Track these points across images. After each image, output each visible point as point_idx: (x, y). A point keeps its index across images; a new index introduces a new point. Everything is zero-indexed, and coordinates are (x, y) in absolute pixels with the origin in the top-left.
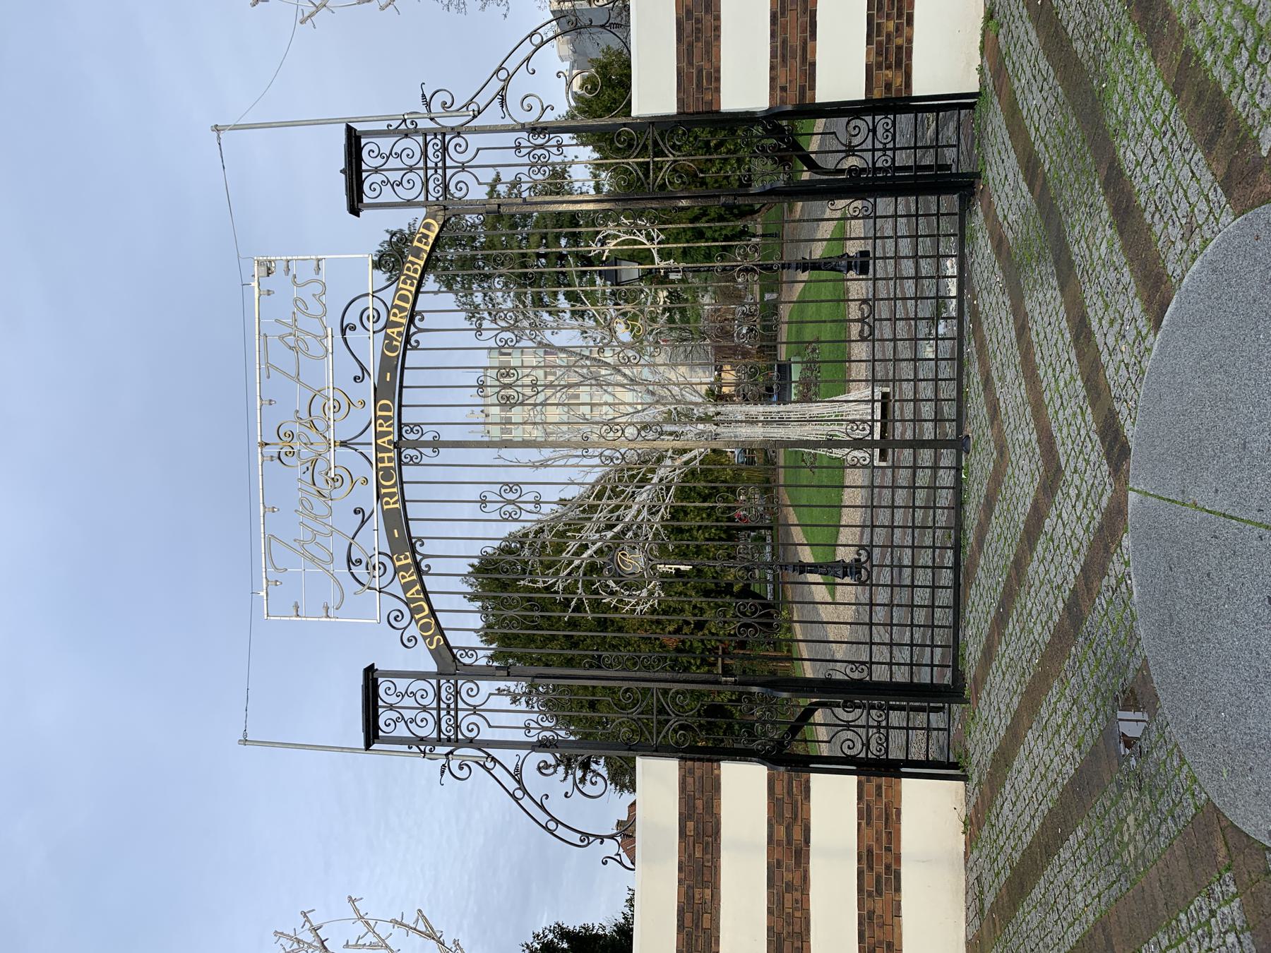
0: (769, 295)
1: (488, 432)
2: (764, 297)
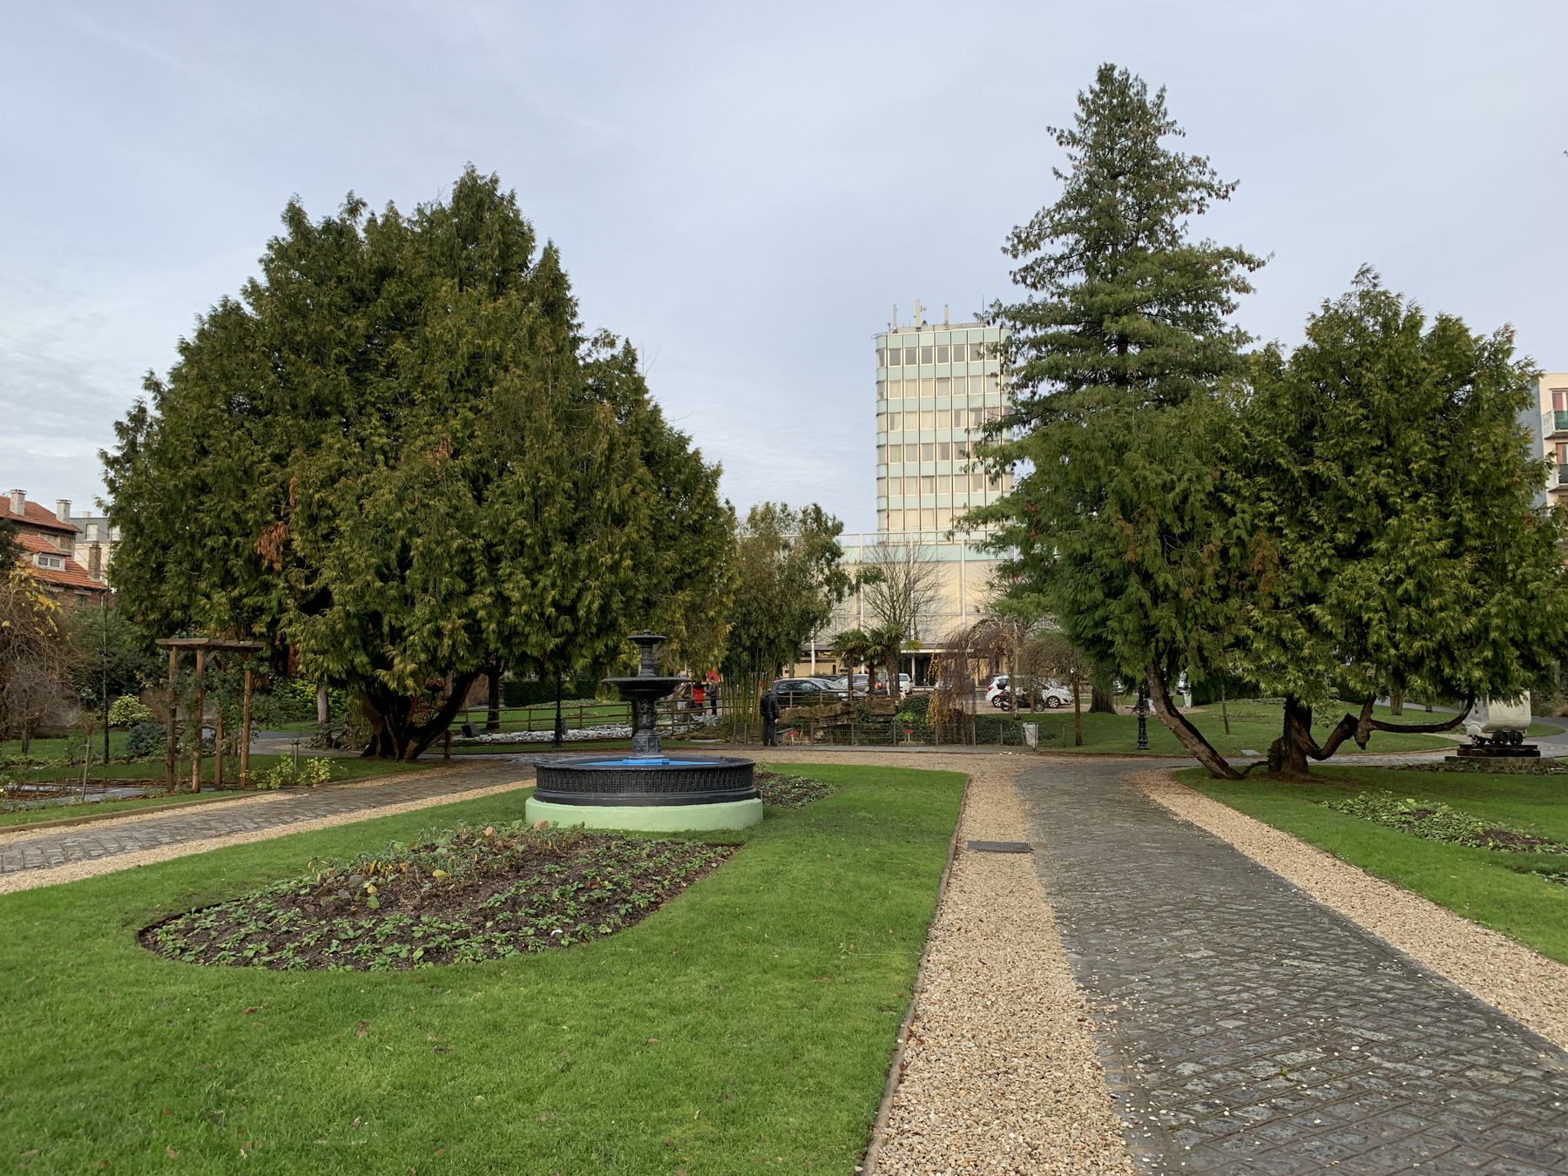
0: (1032, 731)
1: (896, 332)
2: (1029, 722)
